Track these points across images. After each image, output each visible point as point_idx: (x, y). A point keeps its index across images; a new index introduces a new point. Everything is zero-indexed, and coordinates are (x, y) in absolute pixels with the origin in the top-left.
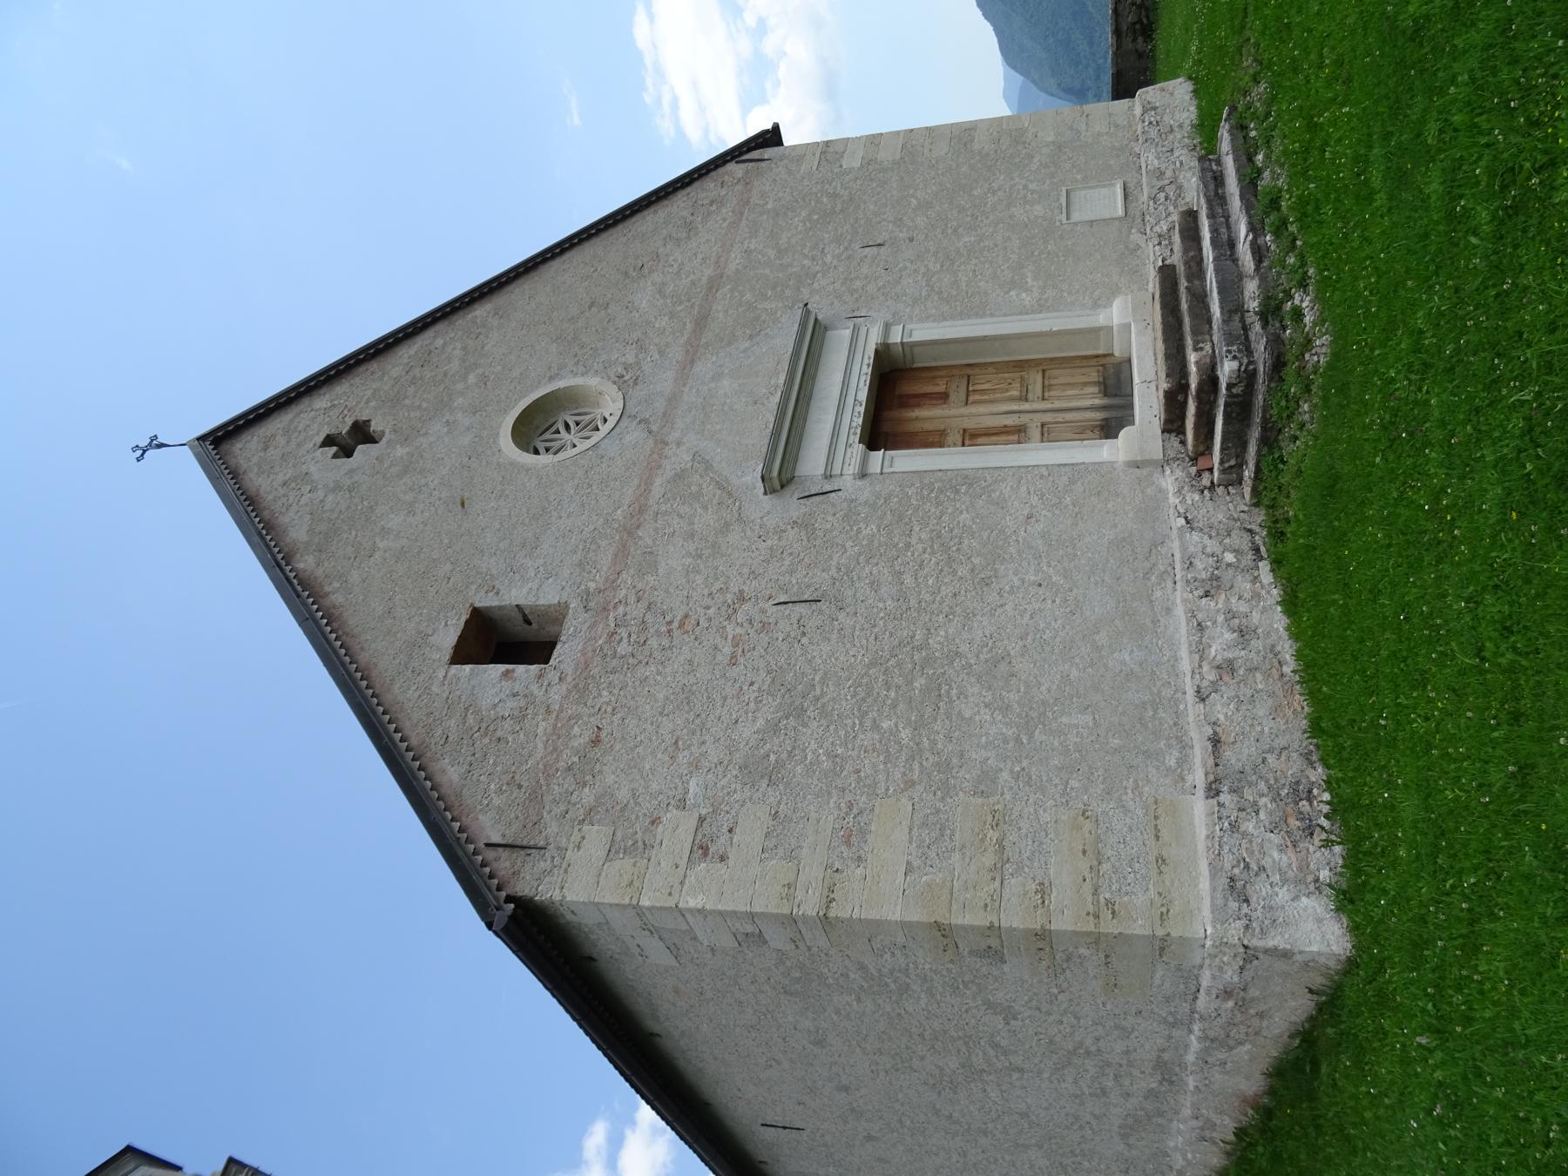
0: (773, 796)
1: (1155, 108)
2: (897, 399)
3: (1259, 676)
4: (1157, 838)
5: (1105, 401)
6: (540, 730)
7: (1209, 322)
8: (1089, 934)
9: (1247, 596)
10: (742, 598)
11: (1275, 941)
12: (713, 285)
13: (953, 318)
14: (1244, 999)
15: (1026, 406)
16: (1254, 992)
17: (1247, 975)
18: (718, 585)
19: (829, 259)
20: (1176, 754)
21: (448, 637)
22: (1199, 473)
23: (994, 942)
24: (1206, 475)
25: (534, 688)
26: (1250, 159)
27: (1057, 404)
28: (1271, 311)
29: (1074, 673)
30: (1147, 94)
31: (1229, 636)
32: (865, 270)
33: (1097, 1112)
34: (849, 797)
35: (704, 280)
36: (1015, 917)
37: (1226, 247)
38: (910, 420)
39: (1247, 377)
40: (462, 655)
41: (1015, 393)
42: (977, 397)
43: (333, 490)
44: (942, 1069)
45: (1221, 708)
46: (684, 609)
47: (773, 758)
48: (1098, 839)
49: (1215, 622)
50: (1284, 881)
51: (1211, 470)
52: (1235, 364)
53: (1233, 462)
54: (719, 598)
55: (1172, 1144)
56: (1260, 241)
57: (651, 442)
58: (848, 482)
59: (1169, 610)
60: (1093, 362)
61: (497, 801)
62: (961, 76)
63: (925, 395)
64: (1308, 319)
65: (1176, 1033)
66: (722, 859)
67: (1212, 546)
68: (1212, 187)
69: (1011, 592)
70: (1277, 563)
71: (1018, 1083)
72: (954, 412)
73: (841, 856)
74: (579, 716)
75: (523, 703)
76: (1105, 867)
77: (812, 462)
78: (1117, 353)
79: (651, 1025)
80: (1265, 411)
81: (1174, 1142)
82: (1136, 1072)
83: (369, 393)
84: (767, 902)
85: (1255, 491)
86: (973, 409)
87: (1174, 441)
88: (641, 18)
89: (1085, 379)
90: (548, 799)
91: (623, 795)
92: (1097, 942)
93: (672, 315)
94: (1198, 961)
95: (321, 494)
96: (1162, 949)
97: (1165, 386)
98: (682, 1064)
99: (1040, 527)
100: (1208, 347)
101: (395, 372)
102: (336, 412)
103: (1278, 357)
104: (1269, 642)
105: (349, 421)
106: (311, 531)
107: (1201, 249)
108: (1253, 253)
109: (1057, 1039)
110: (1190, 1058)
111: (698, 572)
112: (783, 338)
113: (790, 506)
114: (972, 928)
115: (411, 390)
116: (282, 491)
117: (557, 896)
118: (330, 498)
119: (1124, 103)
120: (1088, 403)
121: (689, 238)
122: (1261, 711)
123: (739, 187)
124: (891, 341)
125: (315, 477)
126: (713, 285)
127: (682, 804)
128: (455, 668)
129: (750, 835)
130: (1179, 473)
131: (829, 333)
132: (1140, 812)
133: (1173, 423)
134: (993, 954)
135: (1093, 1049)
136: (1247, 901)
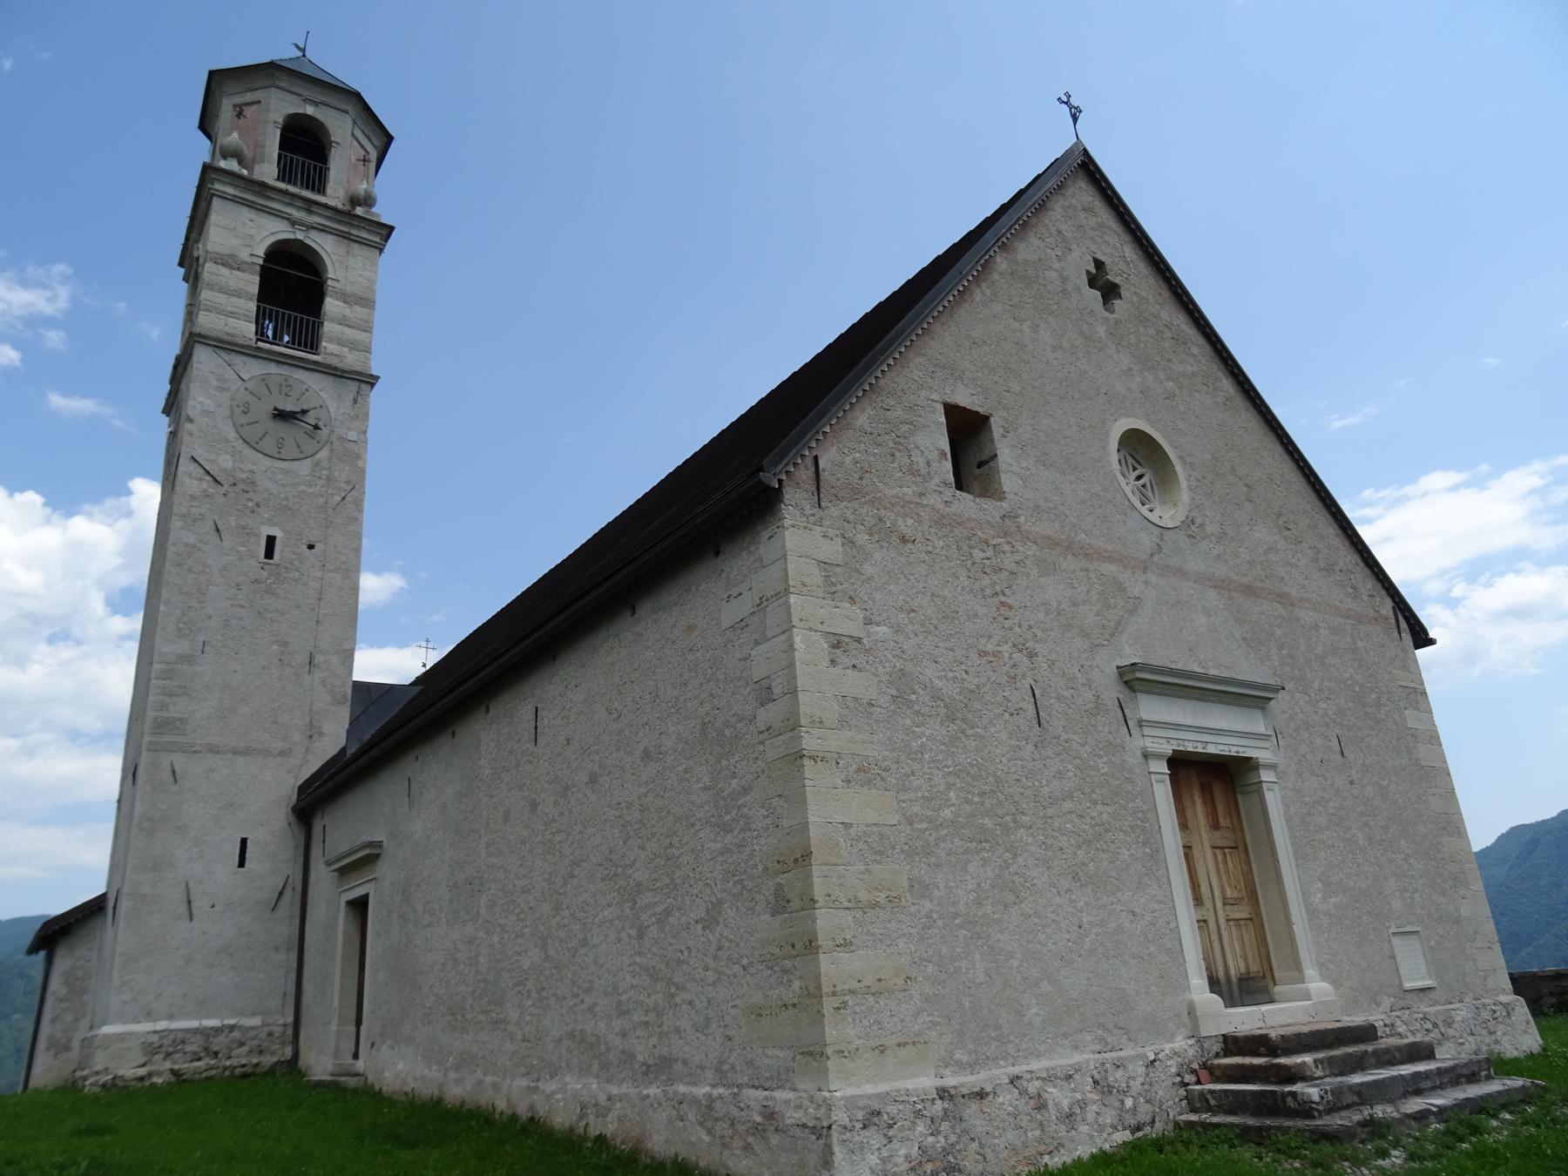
0: (884, 700)
1: (1509, 1015)
2: (1212, 780)
3: (1038, 1133)
4: (899, 1045)
5: (1234, 980)
6: (905, 490)
7: (1341, 1074)
8: (819, 987)
9: (1100, 1120)
10: (1032, 655)
11: (839, 1154)
12: (1282, 597)
13: (1290, 829)
14: (765, 1130)
15: (1219, 905)
16: (775, 1139)
17: (798, 1132)
18: (1039, 633)
19: (1323, 705)
20: (965, 1059)
21: (964, 399)
22: (1193, 1071)
23: (796, 903)
24: (1194, 1079)
25: (936, 480)
26: (1504, 1107)
27: (1225, 934)
28: (1375, 1128)
29: (1015, 963)
30: (1522, 1009)
31: (1065, 1104)
32: (1318, 741)
33: (597, 1009)
34: (894, 767)
35: (1286, 589)
36: (826, 922)
37: (1415, 1086)
38: (1192, 796)
39: (1305, 1110)
40: (952, 411)
41: (1229, 894)
42: (1220, 857)
43: (1061, 276)
44: (632, 865)
45: (1007, 1098)
46: (1015, 604)
47: (913, 697)
48: (891, 992)
49: (1074, 1090)
50: (884, 1160)
51: (1199, 1082)
52: (1316, 1098)
53: (1212, 1102)
54: (1029, 635)
55: (568, 1079)
56: (1432, 1119)
57: (1145, 557)
58: (1138, 743)
59: (1076, 1048)
60: (1266, 966)
61: (848, 460)
63: (1214, 807)
64: (1381, 1162)
65: (709, 1074)
66: (833, 662)
67: (1136, 1085)
68: (1465, 1071)
69: (1072, 901)
70: (1133, 1146)
71: (624, 935)
72: (1205, 836)
73: (848, 765)
74: (920, 522)
75: (923, 471)
76: (871, 999)
77: (1150, 708)
78: (1277, 989)
79: (644, 609)
80: (1278, 1128)
81: (573, 1083)
82: (654, 1040)
83: (1143, 293)
84: (808, 705)
85: (1191, 1124)
86: (1209, 854)
87: (1217, 1047)
88: (1453, 478)
89: (1250, 959)
90: (856, 504)
91: (869, 569)
92: (809, 995)
93: (1251, 563)
94: (800, 1086)
95: (1056, 265)
96: (811, 1054)
97: (1273, 1034)
98: (602, 634)
99: (1127, 924)
100: (1319, 1073)
101: (1164, 315)
102: (1124, 267)
103: (1336, 1138)
104: (1067, 1143)
105: (1117, 280)
106: (1026, 262)
107: (1402, 1063)
108: (1420, 1112)
109: (685, 967)
110: (682, 1088)
111: (1047, 614)
112: (1248, 669)
113: (1111, 691)
114: (811, 885)
115: (1152, 332)
116: (1053, 230)
117: (787, 523)
118: (1055, 275)
119: (1508, 984)
120: (1230, 963)
121: (1320, 570)
122: (1011, 1135)
123: (1371, 613)
124: (1262, 772)
125: (1069, 258)
126: (1282, 597)
127: (868, 622)
128: (941, 408)
129: (861, 685)
130: (1191, 1052)
131: (1259, 713)
132: (916, 1028)
133: (1232, 1044)
134: (780, 904)
135: (678, 1000)
136: (865, 1127)
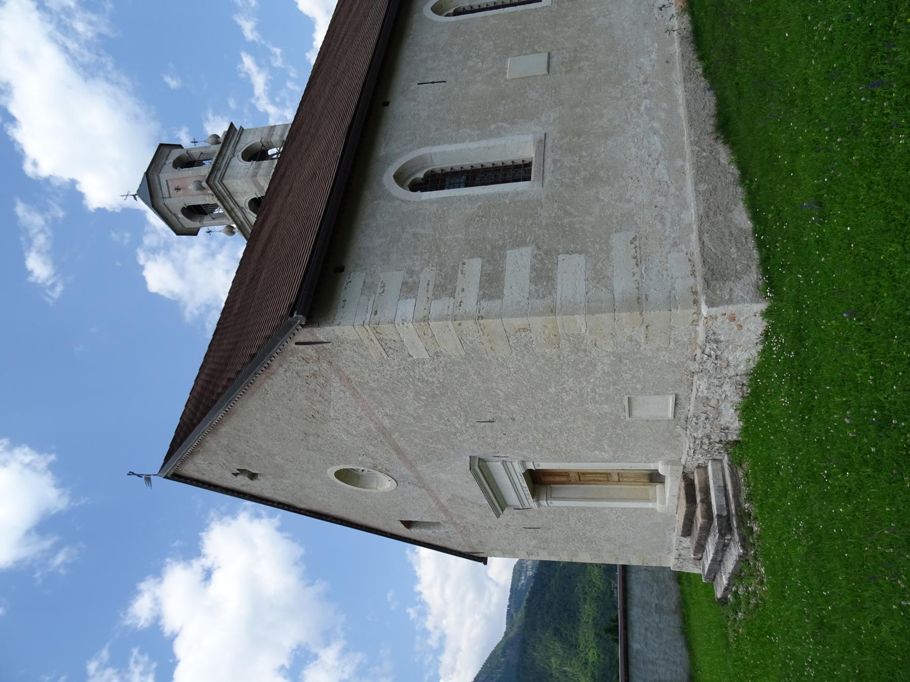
1: (717, 341)
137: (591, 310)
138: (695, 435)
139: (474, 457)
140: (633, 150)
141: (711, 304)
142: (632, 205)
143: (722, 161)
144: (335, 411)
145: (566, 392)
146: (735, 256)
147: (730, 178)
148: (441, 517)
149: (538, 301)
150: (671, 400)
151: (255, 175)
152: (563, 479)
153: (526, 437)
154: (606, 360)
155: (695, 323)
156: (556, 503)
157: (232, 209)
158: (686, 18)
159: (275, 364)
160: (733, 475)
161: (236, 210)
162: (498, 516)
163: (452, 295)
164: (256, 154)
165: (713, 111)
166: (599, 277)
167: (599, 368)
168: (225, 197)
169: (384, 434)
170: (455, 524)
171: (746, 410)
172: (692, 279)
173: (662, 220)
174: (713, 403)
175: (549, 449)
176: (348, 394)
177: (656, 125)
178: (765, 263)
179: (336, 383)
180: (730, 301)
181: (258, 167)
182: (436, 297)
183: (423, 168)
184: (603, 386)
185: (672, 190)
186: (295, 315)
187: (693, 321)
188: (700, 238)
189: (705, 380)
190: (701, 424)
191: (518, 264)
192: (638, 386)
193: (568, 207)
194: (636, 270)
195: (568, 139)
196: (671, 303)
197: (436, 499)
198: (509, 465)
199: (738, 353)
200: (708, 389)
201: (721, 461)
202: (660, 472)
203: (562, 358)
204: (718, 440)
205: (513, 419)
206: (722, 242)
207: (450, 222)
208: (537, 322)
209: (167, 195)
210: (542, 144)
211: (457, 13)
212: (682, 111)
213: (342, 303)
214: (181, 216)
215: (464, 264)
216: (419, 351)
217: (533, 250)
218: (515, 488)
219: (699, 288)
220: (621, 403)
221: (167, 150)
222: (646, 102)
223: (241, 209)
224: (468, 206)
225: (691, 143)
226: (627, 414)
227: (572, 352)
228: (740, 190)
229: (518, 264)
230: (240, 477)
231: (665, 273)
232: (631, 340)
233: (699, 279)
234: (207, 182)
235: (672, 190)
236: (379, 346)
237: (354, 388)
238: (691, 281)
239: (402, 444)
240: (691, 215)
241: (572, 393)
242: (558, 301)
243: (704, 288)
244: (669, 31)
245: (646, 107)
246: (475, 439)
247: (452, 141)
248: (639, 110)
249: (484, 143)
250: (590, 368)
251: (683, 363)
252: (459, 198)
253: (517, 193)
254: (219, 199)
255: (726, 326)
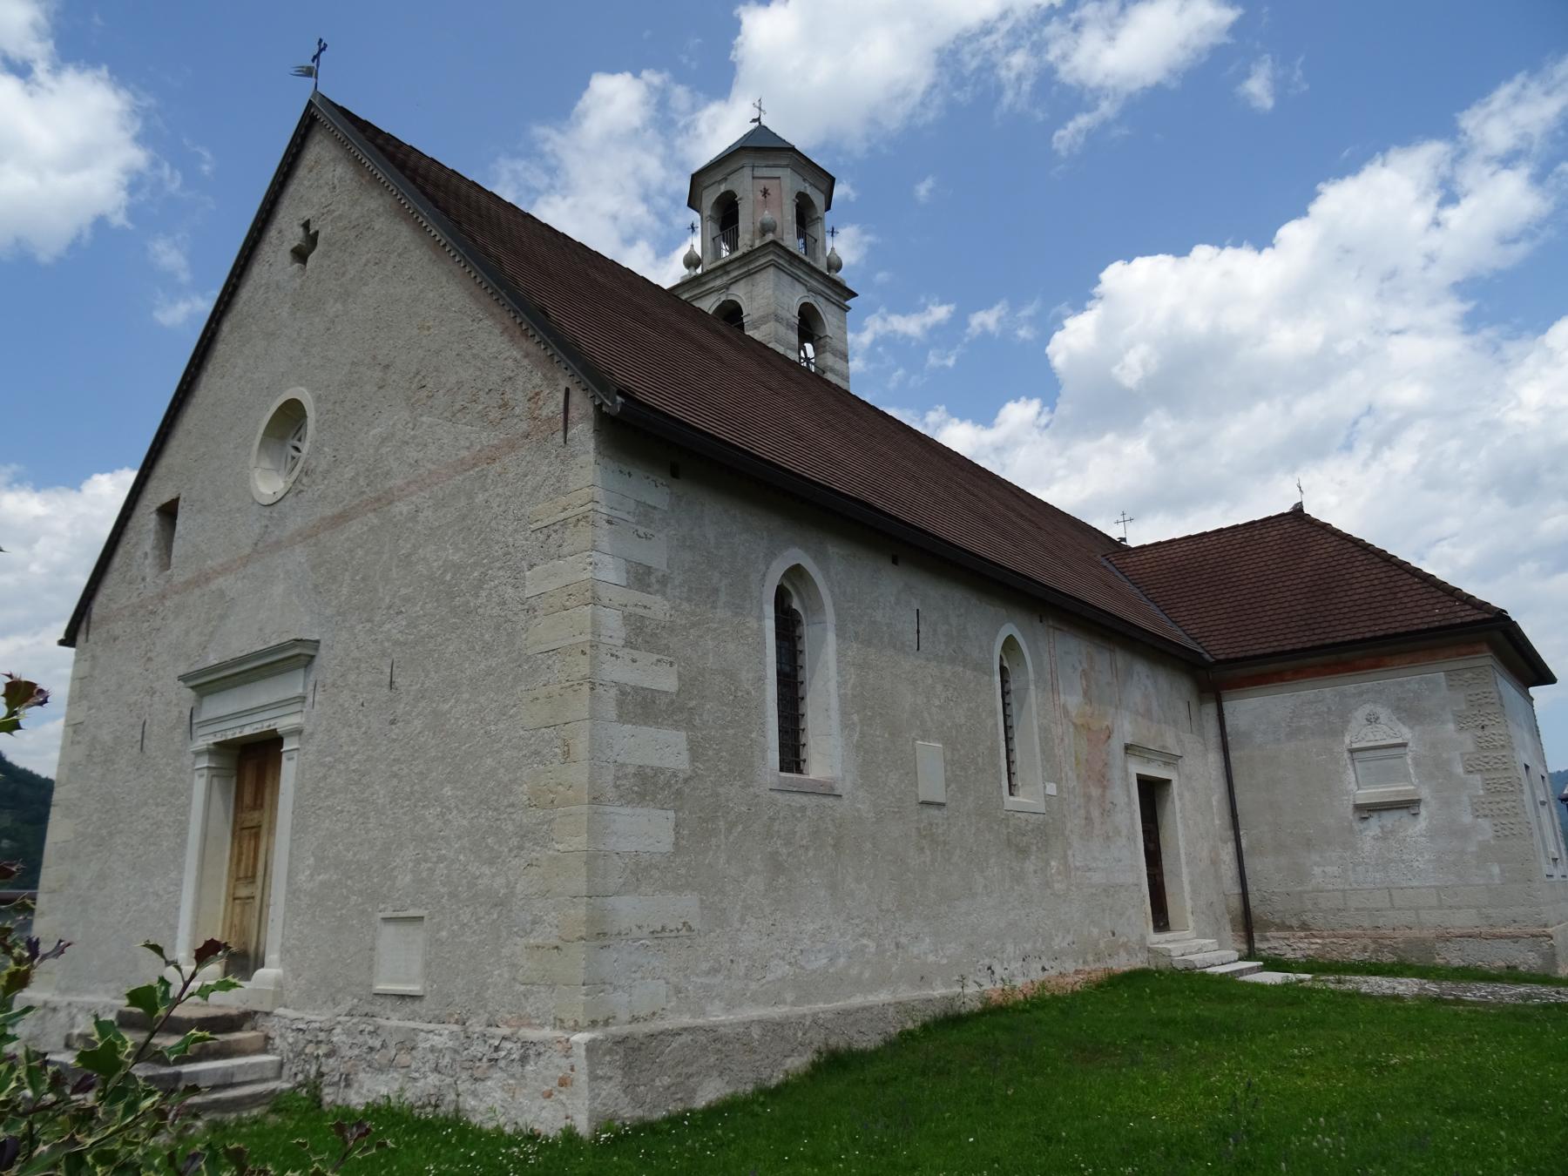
1: (524, 1060)
62: (1555, 765)
137: (593, 859)
138: (338, 1030)
139: (317, 649)
140: (811, 927)
141: (591, 1047)
142: (737, 925)
143: (789, 1061)
144: (430, 426)
145: (442, 814)
146: (658, 1083)
147: (766, 1073)
148: (180, 572)
149: (610, 778)
150: (414, 988)
151: (778, 319)
152: (248, 799)
153: (354, 742)
154: (500, 881)
155: (559, 1023)
156: (199, 785)
157: (727, 273)
158: (977, 1006)
159: (530, 346)
160: (255, 1099)
161: (725, 279)
162: (181, 678)
163: (628, 644)
164: (808, 325)
165: (855, 1046)
166: (641, 872)
167: (486, 870)
168: (747, 265)
169: (379, 500)
170: (163, 597)
171: (386, 1116)
172: (628, 1017)
173: (714, 971)
174: (404, 1058)
175: (325, 777)
176: (464, 453)
177: (842, 961)
178: (646, 1129)
179: (489, 438)
180: (593, 1077)
181: (789, 326)
182: (627, 618)
183: (805, 609)
184: (448, 876)
185: (753, 986)
186: (619, 399)
187: (562, 1021)
188: (685, 1029)
189: (450, 1044)
190: (360, 1039)
191: (665, 748)
192: (444, 934)
193: (740, 828)
194: (646, 931)
195: (832, 829)
196: (596, 984)
197: (225, 570)
198: (297, 707)
199: (498, 1095)
200: (432, 1049)
201: (278, 1076)
202: (260, 972)
203: (510, 810)
204: (324, 1069)
205: (393, 722)
206: (678, 1064)
207: (731, 647)
208: (578, 774)
209: (758, 173)
210: (827, 791)
211: (1003, 670)
212: (857, 1000)
213: (626, 469)
214: (723, 188)
215: (671, 664)
216: (537, 582)
217: (683, 771)
218: (241, 714)
219: (613, 1029)
220: (413, 905)
221: (824, 187)
222: (872, 947)
223: (727, 287)
224: (750, 676)
225: (815, 1014)
226: (388, 914)
227: (520, 826)
228: (749, 1088)
229: (665, 748)
230: (300, 231)
231: (639, 975)
232: (534, 923)
233: (626, 1029)
234: (774, 243)
235: (753, 986)
236: (552, 520)
237: (475, 465)
238: (624, 1016)
239: (355, 527)
240: (717, 1016)
241: (439, 823)
242: (608, 809)
243: (614, 1036)
244: (962, 981)
245: (866, 946)
246: (356, 654)
247: (841, 655)
248: (862, 935)
249: (834, 703)
250: (486, 855)
251: (484, 1007)
252: (762, 663)
253: (764, 751)
254: (744, 255)
255: (554, 1072)
